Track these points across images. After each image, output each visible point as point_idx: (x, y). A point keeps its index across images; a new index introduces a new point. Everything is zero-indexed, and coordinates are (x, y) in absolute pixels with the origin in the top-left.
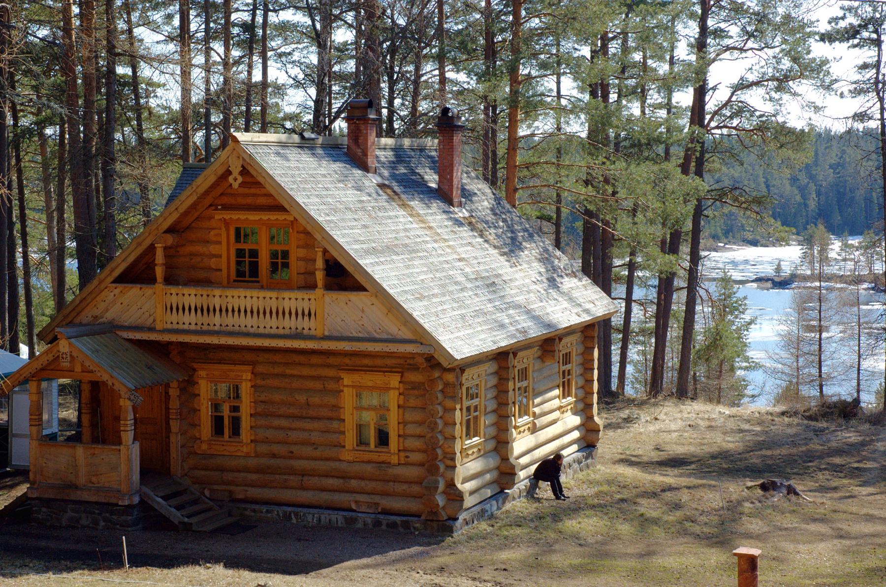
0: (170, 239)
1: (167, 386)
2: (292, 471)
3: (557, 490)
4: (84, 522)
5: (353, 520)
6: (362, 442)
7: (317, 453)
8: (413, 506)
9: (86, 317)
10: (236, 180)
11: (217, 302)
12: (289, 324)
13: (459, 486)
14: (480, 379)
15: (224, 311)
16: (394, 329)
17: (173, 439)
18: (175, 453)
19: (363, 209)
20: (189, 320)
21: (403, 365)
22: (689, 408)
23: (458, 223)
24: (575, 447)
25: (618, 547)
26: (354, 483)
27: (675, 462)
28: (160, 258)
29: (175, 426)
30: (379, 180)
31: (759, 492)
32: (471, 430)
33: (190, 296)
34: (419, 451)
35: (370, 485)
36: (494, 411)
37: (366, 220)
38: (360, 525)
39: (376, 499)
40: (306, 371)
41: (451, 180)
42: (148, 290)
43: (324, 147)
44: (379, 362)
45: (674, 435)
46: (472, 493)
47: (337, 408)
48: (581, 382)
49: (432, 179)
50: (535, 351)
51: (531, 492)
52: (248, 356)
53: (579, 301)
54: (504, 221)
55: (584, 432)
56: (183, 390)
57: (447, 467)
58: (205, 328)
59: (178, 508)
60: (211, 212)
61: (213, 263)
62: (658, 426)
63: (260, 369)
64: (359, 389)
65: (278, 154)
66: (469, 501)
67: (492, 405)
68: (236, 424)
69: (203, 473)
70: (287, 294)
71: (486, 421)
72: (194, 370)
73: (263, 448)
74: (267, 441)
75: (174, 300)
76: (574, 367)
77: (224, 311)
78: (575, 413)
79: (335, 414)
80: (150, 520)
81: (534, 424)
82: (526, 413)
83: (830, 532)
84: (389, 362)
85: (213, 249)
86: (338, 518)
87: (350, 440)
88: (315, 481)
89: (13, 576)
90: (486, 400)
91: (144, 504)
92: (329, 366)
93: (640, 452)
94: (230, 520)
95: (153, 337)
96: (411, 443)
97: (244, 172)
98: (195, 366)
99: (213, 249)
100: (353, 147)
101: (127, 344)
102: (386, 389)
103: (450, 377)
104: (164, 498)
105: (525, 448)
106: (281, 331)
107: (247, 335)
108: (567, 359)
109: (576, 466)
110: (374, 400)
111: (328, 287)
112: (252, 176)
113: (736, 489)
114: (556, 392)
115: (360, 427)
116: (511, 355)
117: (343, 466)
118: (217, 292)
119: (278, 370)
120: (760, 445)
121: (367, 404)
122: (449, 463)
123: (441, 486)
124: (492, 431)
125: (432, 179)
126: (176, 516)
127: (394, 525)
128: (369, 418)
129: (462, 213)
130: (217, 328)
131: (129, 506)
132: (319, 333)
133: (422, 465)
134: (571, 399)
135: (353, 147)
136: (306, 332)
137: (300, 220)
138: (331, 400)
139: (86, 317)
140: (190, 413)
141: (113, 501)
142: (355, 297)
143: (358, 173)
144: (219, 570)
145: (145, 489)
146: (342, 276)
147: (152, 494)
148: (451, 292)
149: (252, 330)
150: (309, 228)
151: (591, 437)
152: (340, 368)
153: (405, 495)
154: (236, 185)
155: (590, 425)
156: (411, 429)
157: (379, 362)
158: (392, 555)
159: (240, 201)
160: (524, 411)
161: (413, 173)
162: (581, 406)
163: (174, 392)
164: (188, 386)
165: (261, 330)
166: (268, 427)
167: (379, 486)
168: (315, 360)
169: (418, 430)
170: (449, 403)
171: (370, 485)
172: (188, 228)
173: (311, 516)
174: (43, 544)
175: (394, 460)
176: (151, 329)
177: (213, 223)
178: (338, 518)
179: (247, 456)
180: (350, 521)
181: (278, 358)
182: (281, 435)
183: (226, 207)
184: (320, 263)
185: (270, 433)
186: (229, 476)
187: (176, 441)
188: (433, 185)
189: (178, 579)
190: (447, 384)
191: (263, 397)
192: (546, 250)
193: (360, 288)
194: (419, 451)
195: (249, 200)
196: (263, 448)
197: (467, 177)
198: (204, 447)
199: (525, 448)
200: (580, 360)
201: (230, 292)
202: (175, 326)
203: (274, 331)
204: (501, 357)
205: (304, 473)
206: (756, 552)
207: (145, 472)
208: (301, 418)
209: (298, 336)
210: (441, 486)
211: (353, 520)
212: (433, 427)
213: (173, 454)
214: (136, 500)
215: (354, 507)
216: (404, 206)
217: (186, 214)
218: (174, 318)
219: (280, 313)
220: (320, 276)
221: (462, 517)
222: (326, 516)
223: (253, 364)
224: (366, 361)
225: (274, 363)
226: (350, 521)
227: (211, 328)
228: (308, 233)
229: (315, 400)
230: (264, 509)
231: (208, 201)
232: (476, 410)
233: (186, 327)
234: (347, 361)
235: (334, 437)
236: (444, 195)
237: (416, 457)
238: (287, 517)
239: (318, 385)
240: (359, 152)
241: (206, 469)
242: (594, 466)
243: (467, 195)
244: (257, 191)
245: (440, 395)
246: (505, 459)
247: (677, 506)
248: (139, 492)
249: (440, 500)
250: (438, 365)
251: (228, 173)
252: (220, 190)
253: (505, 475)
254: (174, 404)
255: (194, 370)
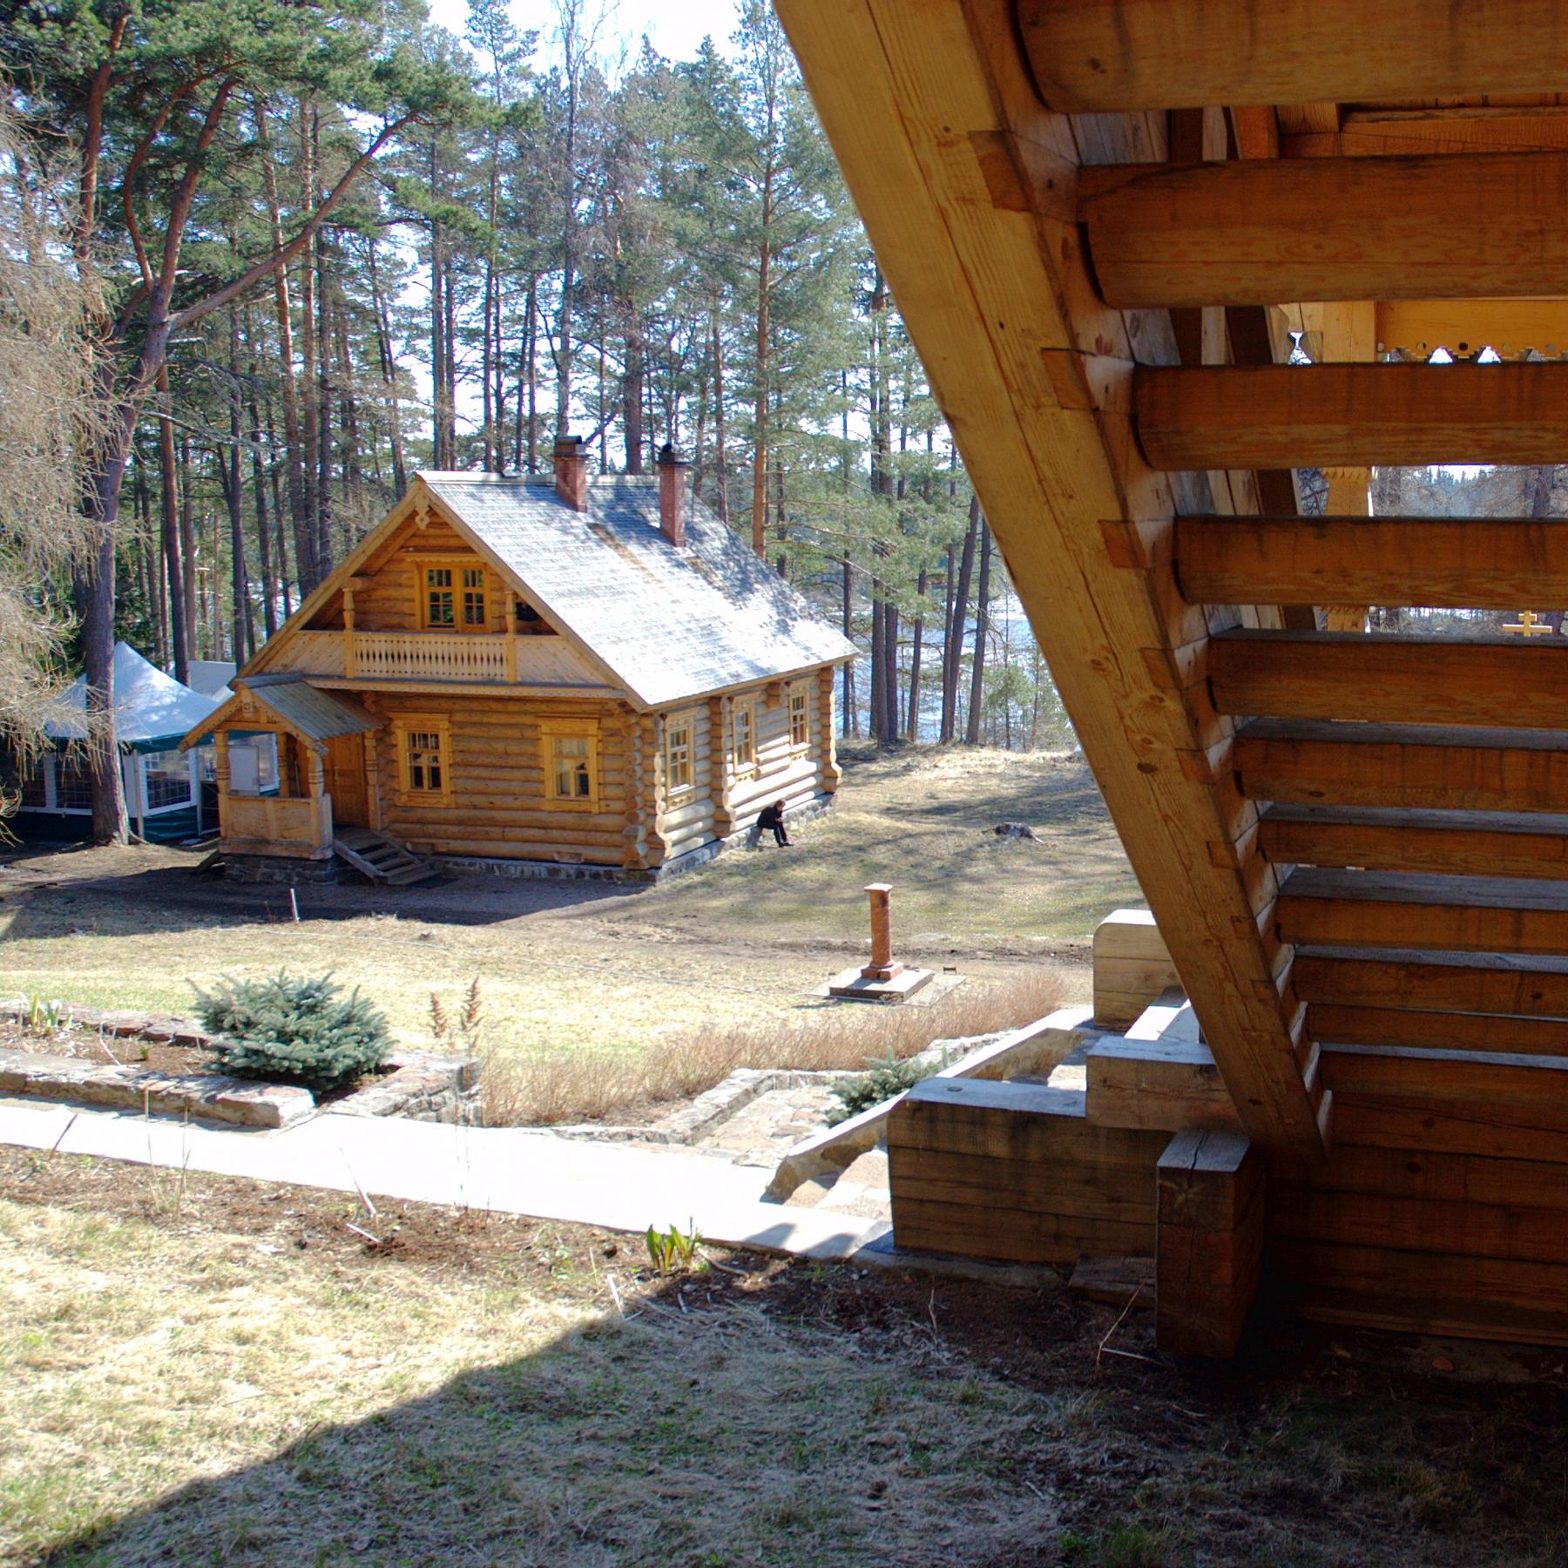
0: (359, 584)
1: (363, 737)
2: (493, 823)
3: (781, 836)
4: (277, 878)
5: (557, 872)
6: (563, 791)
7: (517, 804)
8: (615, 855)
9: (275, 666)
10: (422, 522)
11: (407, 648)
12: (482, 670)
13: (662, 835)
14: (693, 723)
15: (415, 657)
16: (588, 675)
17: (371, 791)
18: (374, 805)
19: (565, 549)
20: (380, 668)
21: (600, 711)
22: (974, 754)
23: (680, 565)
24: (812, 794)
25: (833, 893)
26: (555, 834)
27: (943, 810)
28: (348, 603)
29: (372, 778)
30: (591, 521)
31: (995, 836)
32: (679, 775)
33: (380, 642)
34: (619, 799)
35: (572, 835)
36: (707, 758)
37: (566, 561)
38: (563, 876)
39: (580, 849)
40: (503, 719)
41: (673, 520)
42: (337, 636)
43: (529, 485)
44: (576, 708)
45: (950, 783)
46: (675, 844)
47: (535, 756)
48: (817, 727)
49: (655, 519)
50: (758, 696)
51: (752, 841)
52: (445, 704)
53: (820, 641)
54: (737, 562)
55: (821, 777)
56: (379, 740)
57: (648, 815)
58: (397, 675)
59: (374, 862)
60: (402, 554)
61: (406, 607)
62: (936, 773)
63: (458, 717)
64: (559, 737)
65: (472, 495)
66: (671, 852)
67: (705, 751)
68: (435, 773)
69: (404, 826)
70: (477, 639)
71: (697, 769)
72: (391, 720)
73: (463, 800)
74: (466, 792)
75: (364, 647)
76: (809, 712)
77: (415, 657)
78: (811, 760)
79: (533, 764)
80: (353, 878)
81: (758, 771)
82: (749, 759)
83: (1055, 873)
84: (587, 708)
85: (406, 593)
86: (541, 869)
87: (550, 789)
88: (517, 832)
89: (181, 930)
90: (696, 746)
91: (337, 857)
92: (526, 713)
93: (909, 800)
94: (432, 873)
95: (343, 685)
96: (612, 791)
97: (431, 511)
98: (391, 715)
99: (406, 593)
100: (563, 485)
101: (318, 694)
102: (584, 736)
103: (648, 723)
104: (358, 852)
105: (744, 793)
106: (473, 678)
107: (439, 682)
108: (799, 703)
109: (810, 813)
110: (571, 746)
111: (520, 631)
112: (439, 516)
113: (974, 835)
114: (786, 738)
115: (561, 778)
116: (724, 701)
117: (544, 816)
118: (407, 638)
119: (475, 718)
120: (1038, 791)
121: (561, 751)
122: (650, 811)
123: (642, 834)
124: (705, 779)
125: (655, 519)
126: (371, 870)
127: (596, 876)
128: (569, 766)
129: (684, 553)
130: (408, 676)
131: (321, 861)
132: (511, 679)
133: (622, 813)
134: (805, 745)
135: (563, 485)
136: (498, 678)
137: (491, 564)
138: (529, 749)
139: (275, 666)
140: (387, 763)
141: (305, 855)
142: (544, 640)
143: (566, 513)
144: (391, 921)
145: (338, 843)
146: (533, 619)
147: (346, 848)
148: (656, 636)
149: (444, 678)
150: (498, 570)
151: (829, 784)
152: (536, 715)
153: (607, 845)
154: (422, 526)
155: (828, 773)
156: (611, 777)
157: (576, 708)
158: (588, 905)
159: (433, 542)
160: (745, 754)
161: (635, 512)
162: (817, 752)
163: (370, 743)
164: (385, 733)
165: (453, 677)
166: (468, 778)
167: (581, 836)
168: (512, 707)
169: (618, 778)
170: (648, 750)
171: (572, 835)
172: (380, 571)
173: (514, 869)
174: (231, 899)
175: (595, 809)
176: (342, 678)
177: (405, 566)
178: (541, 869)
179: (448, 808)
180: (553, 873)
181: (474, 705)
182: (480, 785)
183: (418, 549)
184: (510, 607)
185: (470, 784)
186: (430, 829)
187: (374, 794)
188: (657, 525)
189: (346, 930)
190: (645, 730)
191: (461, 747)
192: (782, 593)
193: (552, 632)
194: (619, 799)
195: (441, 542)
196: (463, 800)
197: (693, 512)
198: (404, 798)
199: (744, 793)
200: (816, 704)
201: (420, 638)
202: (366, 674)
203: (466, 678)
204: (712, 701)
205: (505, 825)
206: (885, 887)
207: (339, 826)
208: (501, 767)
209: (490, 682)
210: (642, 834)
211: (557, 872)
212: (631, 774)
213: (372, 807)
214: (329, 854)
215: (557, 858)
216: (617, 547)
217: (376, 555)
218: (365, 665)
219: (471, 659)
220: (511, 620)
221: (665, 867)
222: (529, 868)
223: (450, 712)
224: (563, 708)
225: (472, 711)
226: (553, 873)
227: (403, 675)
228: (500, 575)
229: (514, 748)
230: (467, 861)
231: (399, 542)
232: (683, 756)
233: (377, 675)
234: (544, 707)
235: (534, 787)
236: (666, 535)
237: (617, 806)
238: (490, 869)
239: (516, 733)
240: (568, 490)
241: (405, 821)
242: (833, 812)
243: (695, 534)
244: (444, 532)
245: (637, 742)
246: (720, 807)
247: (909, 852)
248: (332, 846)
249: (641, 849)
250: (633, 711)
251: (415, 513)
252: (411, 531)
253: (720, 825)
254: (371, 755)
255: (391, 720)
